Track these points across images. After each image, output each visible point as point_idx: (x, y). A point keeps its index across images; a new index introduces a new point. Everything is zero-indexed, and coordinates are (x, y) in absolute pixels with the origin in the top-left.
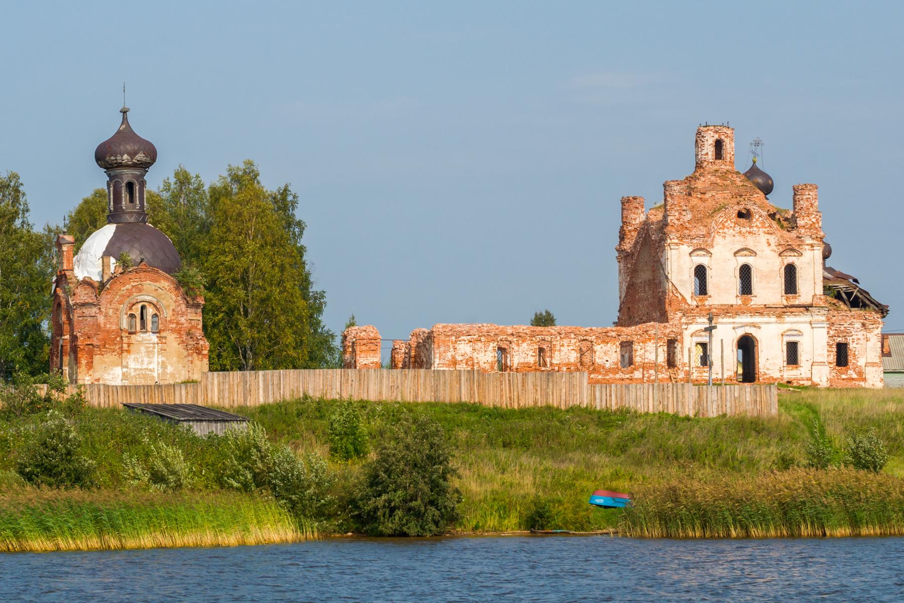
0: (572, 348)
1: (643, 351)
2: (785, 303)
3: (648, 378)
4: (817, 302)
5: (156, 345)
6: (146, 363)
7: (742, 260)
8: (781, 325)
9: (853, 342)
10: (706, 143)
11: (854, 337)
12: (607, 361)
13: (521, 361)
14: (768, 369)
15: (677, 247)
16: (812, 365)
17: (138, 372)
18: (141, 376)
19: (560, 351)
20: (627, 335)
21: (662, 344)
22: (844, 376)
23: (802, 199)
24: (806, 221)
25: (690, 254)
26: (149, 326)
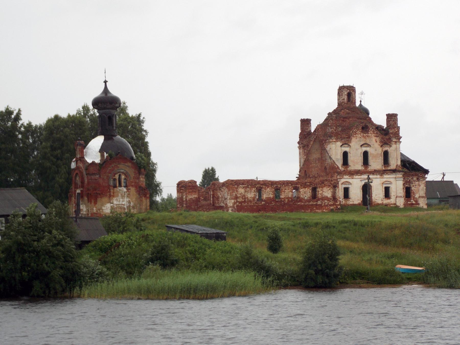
0: (290, 190)
1: (322, 192)
2: (384, 168)
3: (324, 204)
4: (398, 168)
5: (126, 193)
6: (121, 201)
7: (364, 149)
8: (382, 179)
9: (413, 186)
10: (343, 94)
11: (414, 184)
12: (306, 196)
13: (267, 197)
14: (376, 199)
15: (335, 143)
16: (396, 198)
17: (118, 206)
18: (119, 208)
19: (284, 192)
20: (315, 184)
21: (330, 188)
22: (409, 203)
23: (391, 121)
24: (393, 131)
25: (341, 146)
26: (123, 184)
